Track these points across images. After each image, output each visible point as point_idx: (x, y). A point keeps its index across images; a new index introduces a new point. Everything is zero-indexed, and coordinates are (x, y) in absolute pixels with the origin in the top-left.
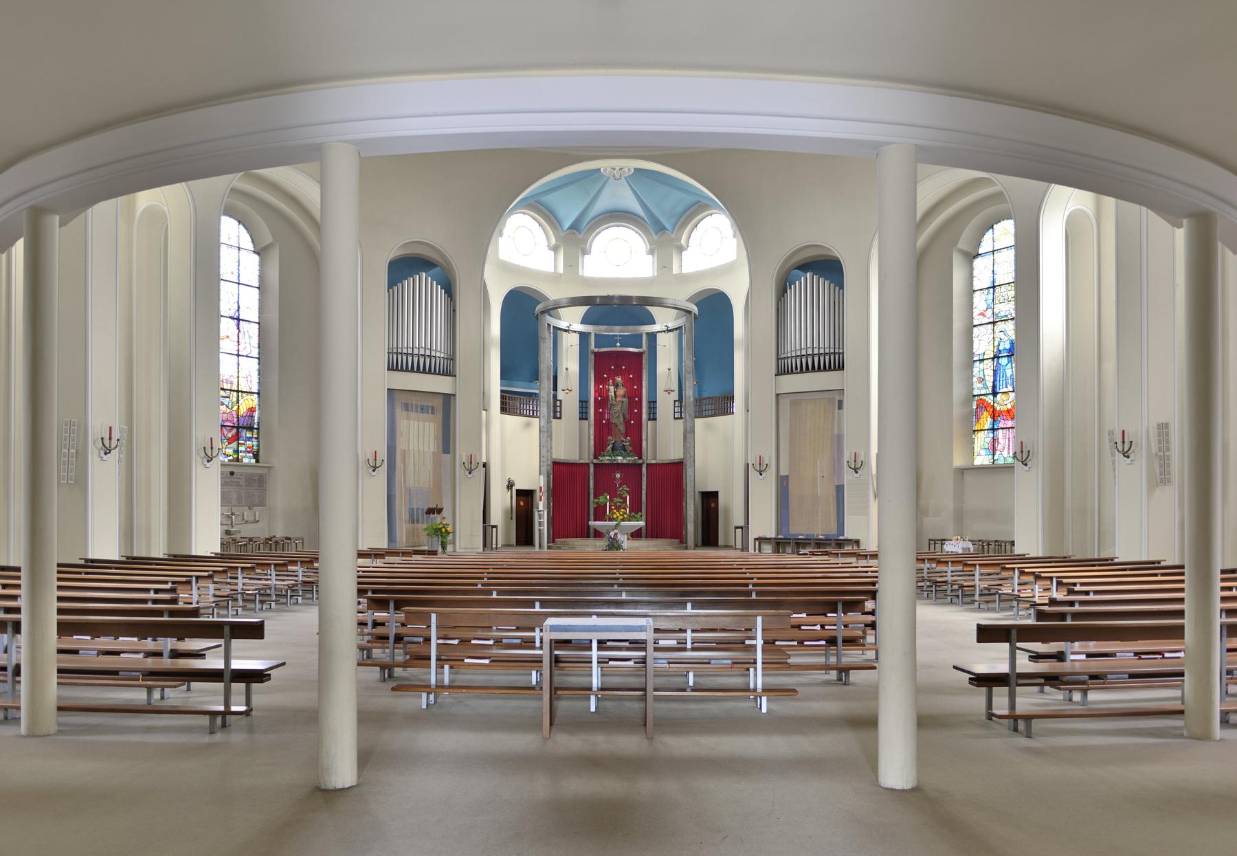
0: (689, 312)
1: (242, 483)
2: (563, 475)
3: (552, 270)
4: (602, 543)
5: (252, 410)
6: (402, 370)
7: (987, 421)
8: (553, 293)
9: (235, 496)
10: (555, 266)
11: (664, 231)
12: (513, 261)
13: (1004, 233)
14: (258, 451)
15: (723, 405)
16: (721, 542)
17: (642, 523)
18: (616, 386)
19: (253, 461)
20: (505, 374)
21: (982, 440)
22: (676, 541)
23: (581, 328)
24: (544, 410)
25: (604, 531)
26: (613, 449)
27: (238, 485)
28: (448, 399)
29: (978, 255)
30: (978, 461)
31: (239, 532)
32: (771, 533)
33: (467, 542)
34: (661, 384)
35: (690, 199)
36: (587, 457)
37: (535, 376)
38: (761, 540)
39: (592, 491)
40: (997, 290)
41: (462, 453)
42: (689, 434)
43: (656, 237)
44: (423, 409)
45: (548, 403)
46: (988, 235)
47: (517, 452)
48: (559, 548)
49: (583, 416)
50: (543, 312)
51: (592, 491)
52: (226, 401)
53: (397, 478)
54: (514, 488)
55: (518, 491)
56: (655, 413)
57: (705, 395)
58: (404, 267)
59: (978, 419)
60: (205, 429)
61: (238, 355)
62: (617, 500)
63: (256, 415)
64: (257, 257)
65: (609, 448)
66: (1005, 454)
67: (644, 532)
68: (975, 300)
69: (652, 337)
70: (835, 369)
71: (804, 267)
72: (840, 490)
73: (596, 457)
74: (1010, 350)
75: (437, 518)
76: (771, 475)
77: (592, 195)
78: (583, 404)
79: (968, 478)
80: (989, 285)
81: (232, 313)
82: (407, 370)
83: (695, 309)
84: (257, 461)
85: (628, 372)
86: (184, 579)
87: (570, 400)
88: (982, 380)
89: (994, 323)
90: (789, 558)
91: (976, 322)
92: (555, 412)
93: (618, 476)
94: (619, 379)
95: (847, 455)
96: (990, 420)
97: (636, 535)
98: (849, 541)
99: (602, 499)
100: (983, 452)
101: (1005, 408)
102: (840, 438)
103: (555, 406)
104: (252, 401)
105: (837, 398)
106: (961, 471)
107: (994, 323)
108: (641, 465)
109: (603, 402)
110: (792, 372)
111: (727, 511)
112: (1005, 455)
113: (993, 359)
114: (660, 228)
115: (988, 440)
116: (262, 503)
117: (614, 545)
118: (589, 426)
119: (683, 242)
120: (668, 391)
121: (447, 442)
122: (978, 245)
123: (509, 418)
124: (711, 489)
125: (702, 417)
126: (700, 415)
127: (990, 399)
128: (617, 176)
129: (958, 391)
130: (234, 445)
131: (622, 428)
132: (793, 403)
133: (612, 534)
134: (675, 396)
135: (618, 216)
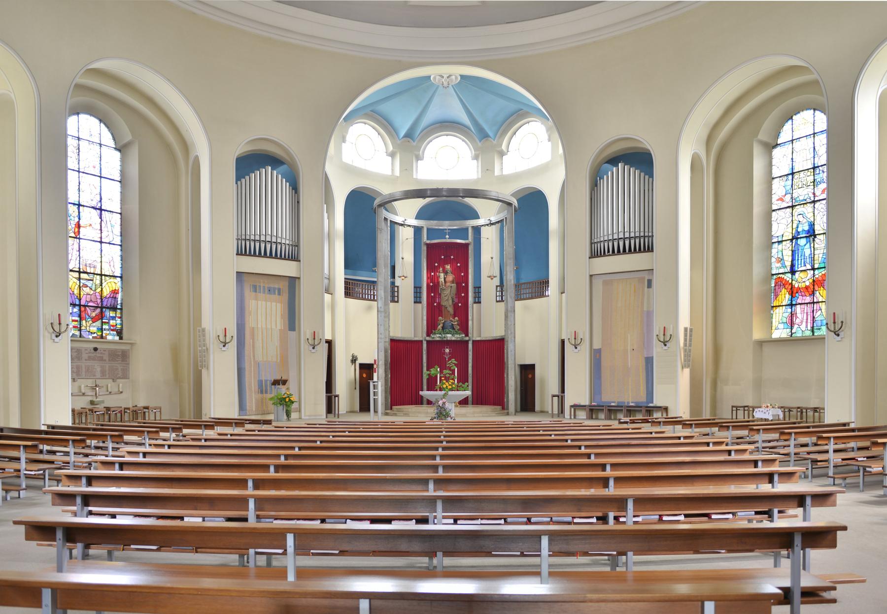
0: (510, 204)
1: (106, 357)
2: (401, 353)
3: (390, 173)
4: (432, 411)
5: (115, 292)
6: (250, 255)
7: (785, 297)
8: (386, 190)
9: (99, 369)
10: (393, 170)
11: (486, 136)
12: (355, 164)
13: (809, 123)
14: (121, 329)
15: (539, 288)
16: (537, 408)
17: (468, 393)
18: (446, 273)
19: (117, 338)
20: (347, 266)
21: (780, 315)
22: (499, 407)
23: (416, 223)
24: (382, 291)
25: (433, 400)
26: (443, 328)
27: (101, 359)
28: (293, 282)
29: (777, 145)
30: (776, 335)
31: (103, 402)
32: (586, 402)
33: (311, 408)
34: (485, 272)
35: (513, 107)
36: (420, 335)
37: (373, 266)
38: (576, 407)
39: (425, 365)
40: (796, 176)
41: (306, 328)
42: (509, 314)
43: (480, 144)
44: (270, 291)
45: (385, 288)
46: (788, 126)
47: (360, 331)
48: (395, 415)
49: (417, 300)
50: (380, 206)
51: (425, 365)
52: (89, 283)
53: (246, 353)
54: (358, 363)
55: (361, 365)
56: (479, 297)
57: (523, 281)
58: (249, 163)
59: (776, 296)
60: (53, 306)
61: (101, 242)
62: (445, 372)
63: (119, 297)
64: (118, 154)
65: (440, 327)
66: (803, 327)
67: (470, 399)
68: (773, 186)
69: (477, 230)
70: (645, 251)
71: (614, 161)
72: (649, 361)
73: (428, 335)
74: (808, 232)
75: (283, 389)
76: (585, 348)
77: (424, 103)
78: (417, 289)
79: (766, 349)
80: (788, 171)
81: (94, 204)
82: (255, 255)
83: (515, 202)
84: (121, 338)
85: (456, 260)
86: (117, 433)
87: (406, 286)
88: (781, 260)
89: (793, 207)
90: (601, 421)
91: (774, 207)
92: (393, 296)
93: (447, 351)
94: (448, 267)
95: (657, 330)
96: (788, 296)
97: (464, 402)
98: (659, 408)
99: (433, 371)
100: (781, 326)
101: (803, 285)
102: (649, 315)
103: (393, 292)
104: (116, 284)
105: (647, 278)
106: (761, 343)
107: (793, 207)
108: (467, 342)
109: (434, 288)
110: (605, 255)
111: (542, 381)
112: (802, 329)
113: (792, 240)
114: (483, 135)
115: (786, 315)
116: (125, 376)
117: (442, 413)
118: (422, 309)
119: (504, 147)
120: (491, 277)
121: (292, 320)
122: (778, 136)
123: (354, 304)
124: (528, 362)
125: (521, 299)
126: (519, 298)
127: (788, 277)
128: (445, 84)
129: (757, 270)
130: (98, 323)
131: (451, 310)
132: (605, 283)
133: (440, 403)
134: (497, 281)
135: (447, 125)
